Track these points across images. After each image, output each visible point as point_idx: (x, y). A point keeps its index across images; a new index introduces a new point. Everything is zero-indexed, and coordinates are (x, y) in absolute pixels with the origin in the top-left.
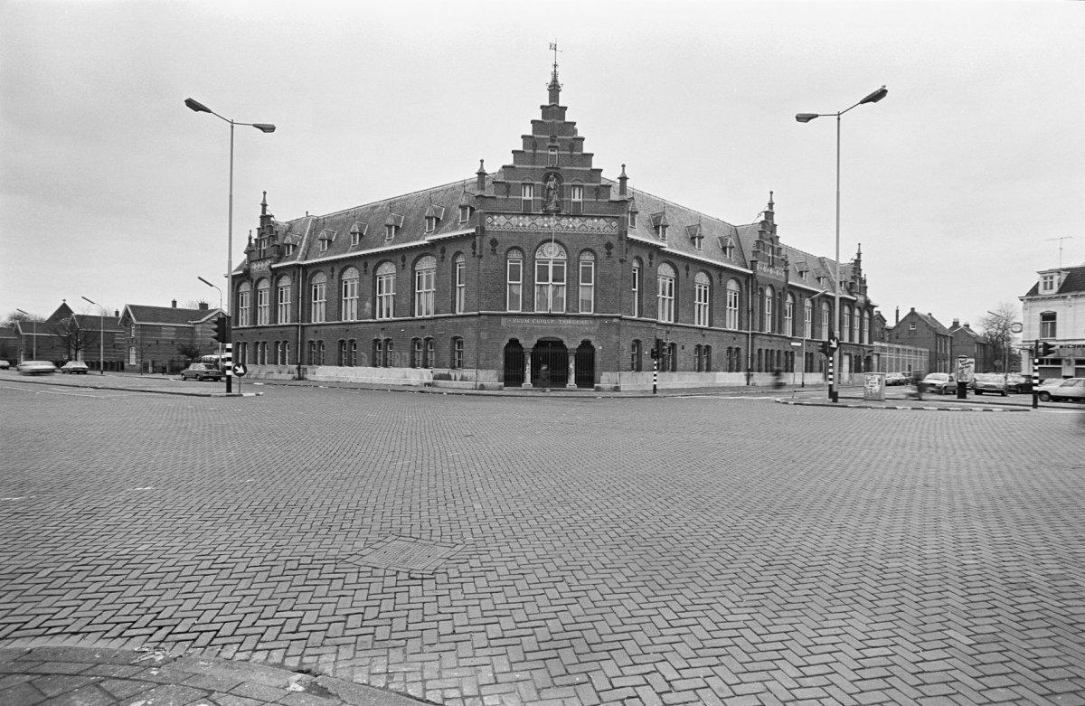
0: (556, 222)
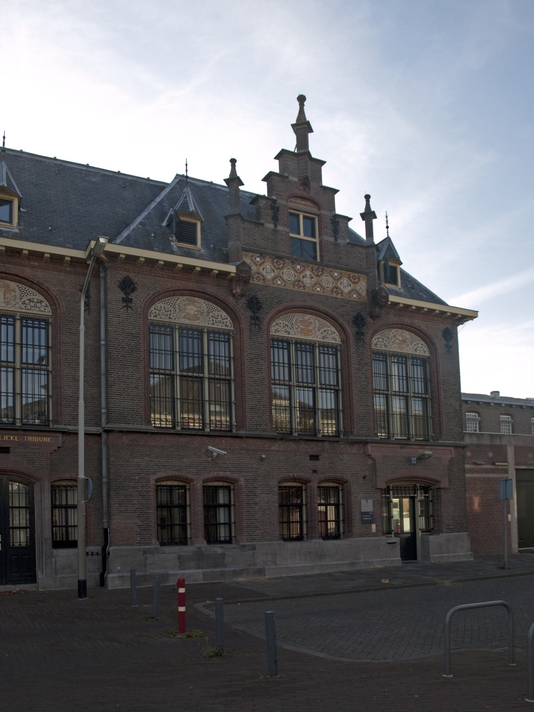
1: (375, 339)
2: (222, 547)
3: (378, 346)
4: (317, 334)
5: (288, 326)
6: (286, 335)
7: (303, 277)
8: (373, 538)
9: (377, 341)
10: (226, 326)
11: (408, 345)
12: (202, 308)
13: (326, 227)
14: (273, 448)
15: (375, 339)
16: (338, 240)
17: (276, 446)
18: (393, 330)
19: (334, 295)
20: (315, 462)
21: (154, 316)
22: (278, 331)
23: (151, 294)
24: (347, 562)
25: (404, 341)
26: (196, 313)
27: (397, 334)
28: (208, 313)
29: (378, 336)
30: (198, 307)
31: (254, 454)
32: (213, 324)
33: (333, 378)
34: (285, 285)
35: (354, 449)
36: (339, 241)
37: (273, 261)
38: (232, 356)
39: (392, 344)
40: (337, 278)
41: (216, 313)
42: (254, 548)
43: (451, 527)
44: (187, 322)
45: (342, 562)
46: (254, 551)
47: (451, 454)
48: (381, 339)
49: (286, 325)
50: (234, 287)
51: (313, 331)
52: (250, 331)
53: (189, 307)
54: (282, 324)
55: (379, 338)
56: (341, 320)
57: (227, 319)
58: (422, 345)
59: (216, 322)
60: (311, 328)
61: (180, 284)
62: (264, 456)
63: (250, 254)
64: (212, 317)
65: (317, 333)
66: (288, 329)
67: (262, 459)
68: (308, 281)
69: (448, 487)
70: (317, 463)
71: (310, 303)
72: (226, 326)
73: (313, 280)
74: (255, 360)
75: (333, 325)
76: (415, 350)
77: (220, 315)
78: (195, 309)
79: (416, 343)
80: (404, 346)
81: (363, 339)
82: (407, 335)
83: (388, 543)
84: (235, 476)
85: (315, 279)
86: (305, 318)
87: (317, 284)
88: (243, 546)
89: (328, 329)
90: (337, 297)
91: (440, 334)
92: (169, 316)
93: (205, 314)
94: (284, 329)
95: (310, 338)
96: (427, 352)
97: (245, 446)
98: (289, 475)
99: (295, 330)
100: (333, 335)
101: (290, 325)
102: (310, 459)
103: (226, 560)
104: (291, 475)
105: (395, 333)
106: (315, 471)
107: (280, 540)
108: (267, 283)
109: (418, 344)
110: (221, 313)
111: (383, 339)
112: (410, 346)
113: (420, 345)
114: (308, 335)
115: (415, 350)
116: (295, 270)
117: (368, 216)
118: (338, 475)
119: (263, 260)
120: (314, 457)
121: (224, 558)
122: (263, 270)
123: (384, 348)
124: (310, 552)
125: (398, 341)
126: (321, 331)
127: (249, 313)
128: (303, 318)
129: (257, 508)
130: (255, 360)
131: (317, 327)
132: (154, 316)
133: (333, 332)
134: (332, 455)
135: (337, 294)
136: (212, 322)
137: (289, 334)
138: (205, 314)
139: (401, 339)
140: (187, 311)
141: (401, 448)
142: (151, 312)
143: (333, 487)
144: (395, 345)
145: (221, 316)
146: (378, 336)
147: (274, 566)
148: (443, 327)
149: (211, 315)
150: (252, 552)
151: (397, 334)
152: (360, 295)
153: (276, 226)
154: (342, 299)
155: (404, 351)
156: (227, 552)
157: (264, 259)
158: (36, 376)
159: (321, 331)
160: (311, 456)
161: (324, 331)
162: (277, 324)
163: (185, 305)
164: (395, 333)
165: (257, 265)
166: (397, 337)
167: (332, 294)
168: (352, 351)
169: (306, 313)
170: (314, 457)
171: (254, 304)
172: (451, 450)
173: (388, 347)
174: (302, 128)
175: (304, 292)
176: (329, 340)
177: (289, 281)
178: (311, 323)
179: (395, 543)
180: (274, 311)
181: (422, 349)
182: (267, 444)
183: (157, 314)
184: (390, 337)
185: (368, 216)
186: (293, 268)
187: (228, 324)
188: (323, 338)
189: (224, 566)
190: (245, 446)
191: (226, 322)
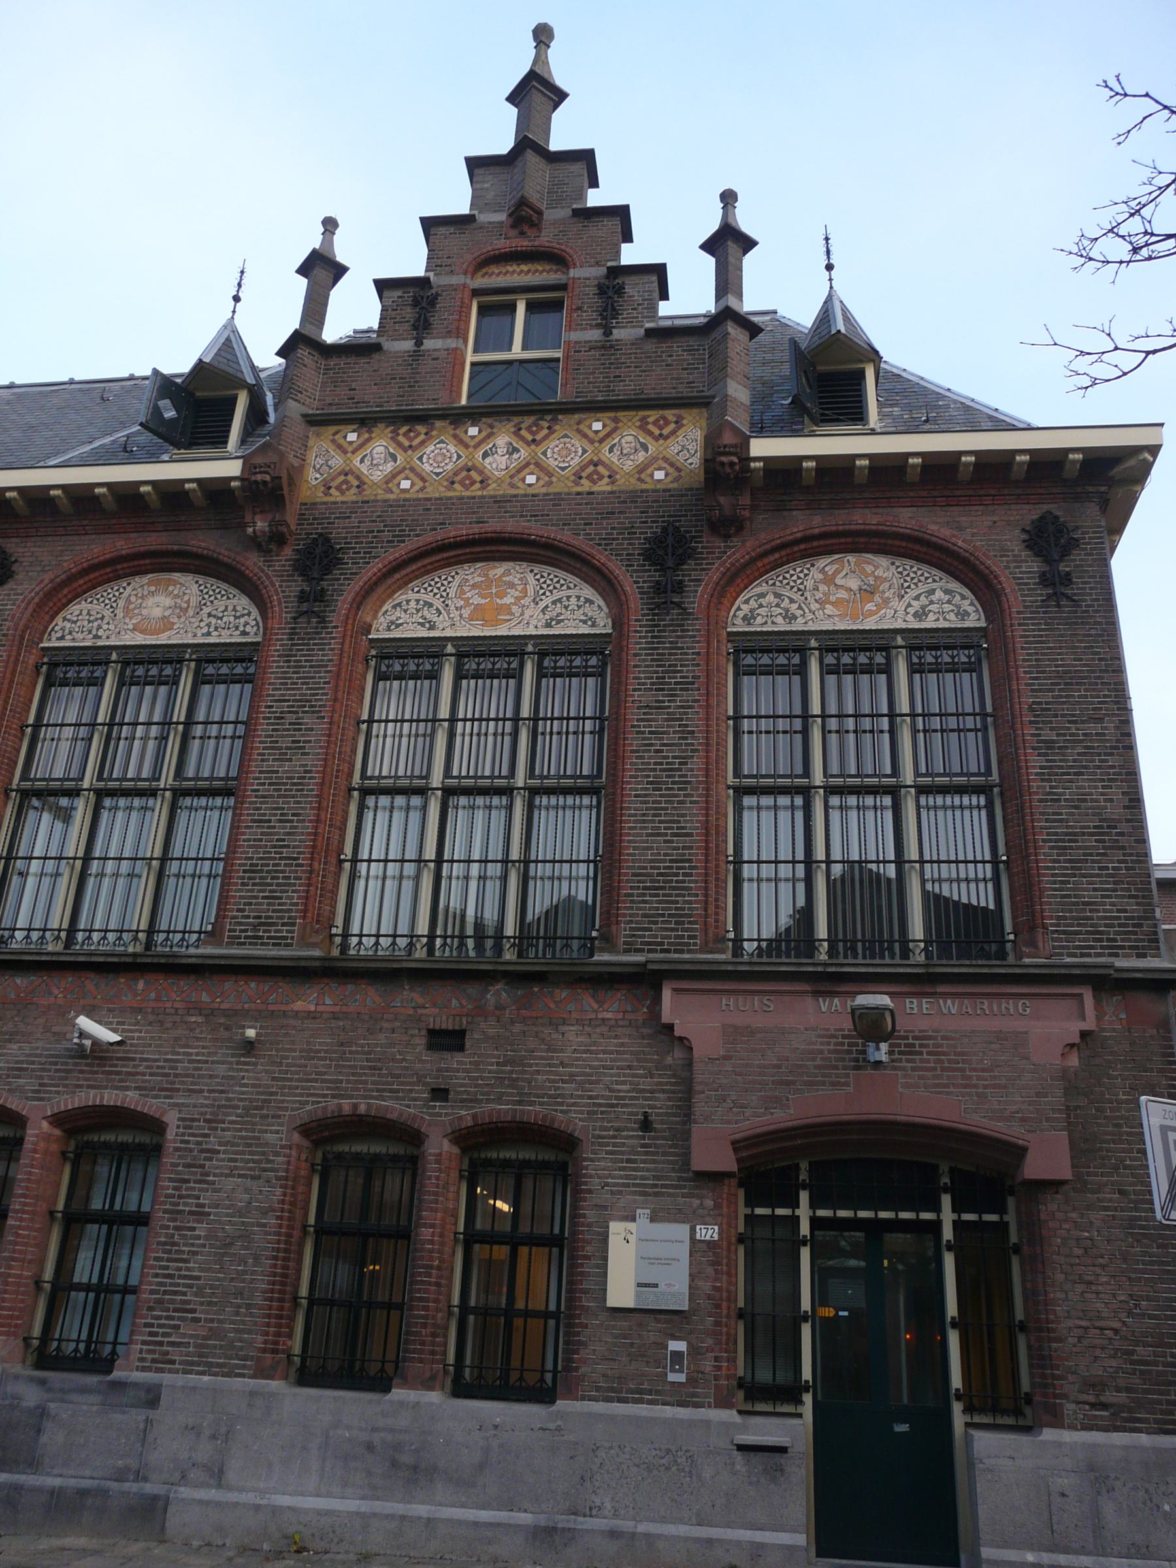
0: (524, 453)
1: (747, 602)
2: (42, 1382)
3: (759, 620)
4: (526, 616)
5: (431, 605)
6: (423, 633)
7: (485, 455)
8: (669, 1411)
9: (753, 604)
10: (244, 633)
11: (886, 601)
12: (186, 598)
13: (579, 309)
14: (299, 1005)
15: (747, 602)
16: (615, 331)
17: (308, 1000)
18: (822, 562)
19: (586, 486)
20: (447, 1055)
21: (58, 639)
22: (398, 626)
23: (46, 581)
24: (525, 1518)
25: (868, 592)
26: (167, 614)
27: (837, 572)
28: (200, 606)
29: (758, 590)
30: (177, 596)
31: (227, 1029)
32: (209, 634)
33: (767, 747)
34: (422, 489)
35: (612, 1007)
36: (617, 334)
37: (395, 433)
38: (989, 709)
39: (815, 606)
40: (601, 435)
41: (221, 604)
42: (152, 1398)
43: (1109, 1397)
44: (139, 639)
45: (502, 1516)
46: (152, 1414)
47: (1083, 1017)
48: (770, 598)
49: (426, 603)
50: (248, 519)
51: (514, 609)
52: (293, 634)
53: (151, 601)
54: (413, 604)
55: (763, 595)
56: (601, 557)
57: (249, 614)
58: (947, 592)
59: (216, 629)
60: (508, 600)
61: (122, 544)
62: (251, 1033)
63: (332, 429)
64: (209, 615)
65: (528, 613)
66: (429, 614)
67: (249, 1046)
68: (498, 463)
69: (1066, 1174)
70: (455, 1060)
71: (511, 525)
72: (244, 633)
73: (515, 456)
74: (291, 718)
75: (586, 582)
76: (916, 615)
77: (230, 608)
78: (168, 602)
79: (922, 588)
80: (870, 606)
81: (678, 605)
82: (882, 567)
83: (741, 1448)
84: (150, 1105)
85: (524, 453)
86: (491, 573)
87: (528, 464)
88: (120, 1385)
89: (569, 593)
90: (595, 489)
91: (1014, 541)
92: (94, 632)
93: (191, 612)
94: (579, 614)
95: (502, 631)
96: (974, 616)
97: (205, 997)
98: (340, 1105)
99: (455, 614)
100: (587, 609)
101: (438, 603)
102: (431, 1047)
103: (44, 1439)
104: (346, 1105)
105: (830, 570)
106: (440, 1094)
107: (261, 1372)
108: (368, 493)
109: (933, 592)
110: (235, 601)
111: (777, 595)
112: (895, 603)
113: (939, 594)
114: (498, 623)
115: (916, 615)
116: (461, 442)
117: (728, 244)
118: (534, 1111)
119: (366, 436)
120: (447, 1040)
121: (39, 1431)
122: (362, 461)
123: (782, 626)
124: (370, 1447)
125: (842, 594)
126: (542, 605)
127: (298, 585)
128: (486, 575)
129: (201, 1229)
130: (291, 718)
131: (530, 592)
132: (58, 639)
133: (587, 600)
134: (517, 1028)
135: (594, 482)
136: (205, 630)
137: (432, 628)
138: (191, 612)
139: (854, 584)
140: (145, 612)
141: (816, 994)
142: (53, 629)
143: (395, 1158)
144: (829, 609)
145: (234, 610)
146: (758, 590)
147: (212, 1494)
148: (1029, 513)
149: (206, 610)
150: (138, 1416)
151: (837, 572)
152: (678, 470)
153: (419, 343)
154: (612, 492)
155: (870, 624)
156: (52, 1405)
157: (370, 432)
158: (870, 815)
159: (542, 605)
160: (432, 1033)
161: (554, 603)
162: (399, 604)
163: (143, 597)
164: (830, 570)
165: (345, 452)
166: (838, 581)
167: (577, 484)
168: (634, 648)
169: (494, 559)
170: (447, 1040)
171: (319, 559)
172: (1081, 995)
173: (800, 620)
174: (536, 93)
175: (483, 497)
176: (572, 627)
177: (437, 474)
178: (512, 585)
179: (782, 1450)
180: (376, 567)
181: (947, 607)
182: (278, 994)
183: (67, 631)
184: (809, 584)
185: (728, 244)
186: (455, 436)
187: (248, 629)
188: (548, 625)
189: (33, 1464)
190: (205, 997)
191: (246, 624)
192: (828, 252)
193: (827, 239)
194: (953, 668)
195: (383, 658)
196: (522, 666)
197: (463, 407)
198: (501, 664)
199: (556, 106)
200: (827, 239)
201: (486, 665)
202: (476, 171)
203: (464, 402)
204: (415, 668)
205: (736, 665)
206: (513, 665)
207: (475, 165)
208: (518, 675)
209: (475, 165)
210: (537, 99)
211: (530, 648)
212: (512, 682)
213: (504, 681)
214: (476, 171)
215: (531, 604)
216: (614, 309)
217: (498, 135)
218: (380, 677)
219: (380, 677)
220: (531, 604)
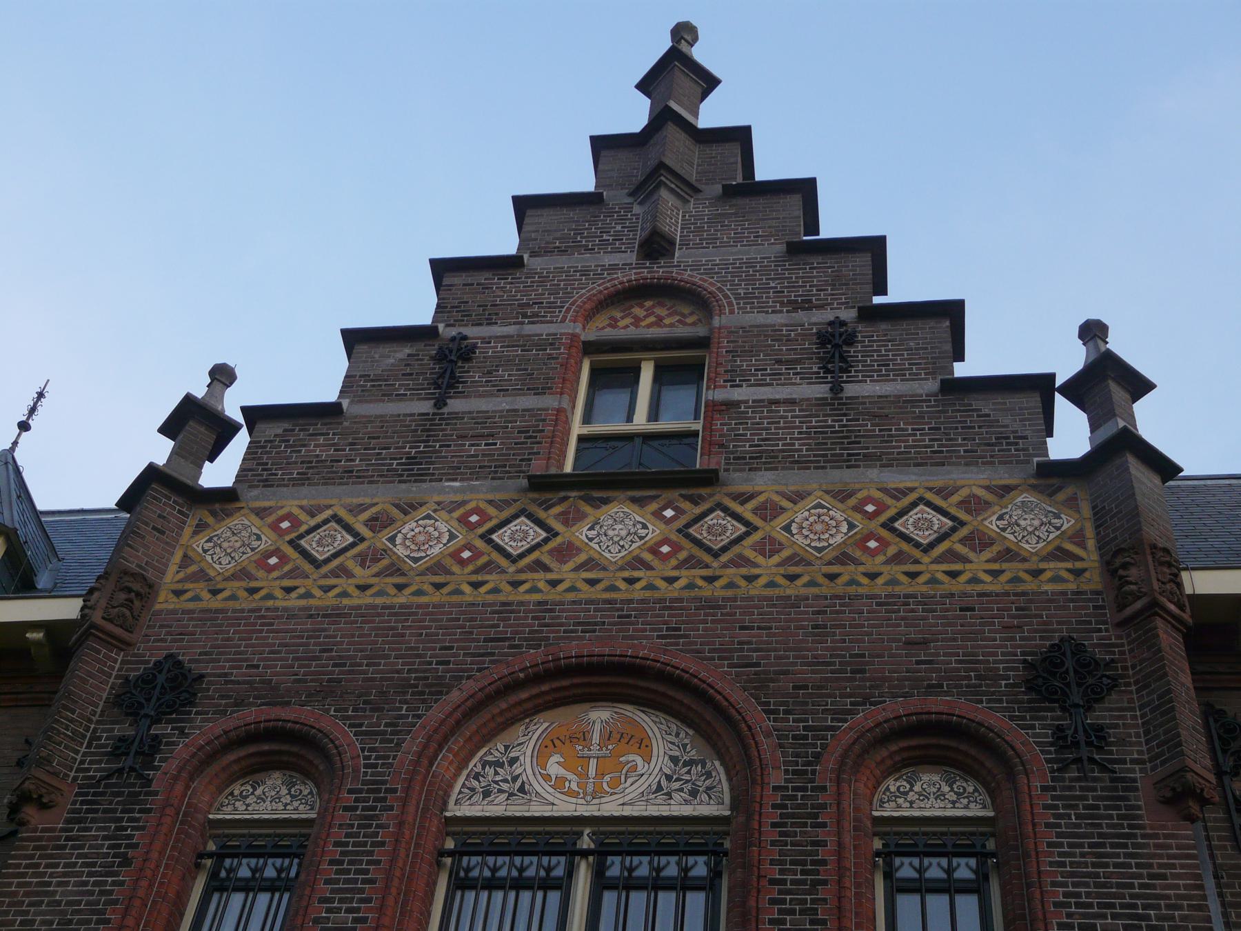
36: (851, 390)
192: (32, 410)
193: (41, 395)
194: (950, 887)
195: (463, 854)
196: (571, 872)
197: (567, 475)
198: (532, 866)
199: (705, 95)
200: (41, 395)
201: (505, 866)
202: (603, 153)
203: (568, 468)
204: (248, 874)
205: (888, 876)
206: (559, 872)
207: (601, 145)
208: (564, 885)
209: (601, 145)
210: (684, 81)
211: (586, 843)
212: (554, 897)
213: (540, 894)
214: (603, 153)
215: (636, 773)
216: (843, 359)
217: (633, 115)
218: (461, 883)
219: (461, 883)
220: (636, 773)
